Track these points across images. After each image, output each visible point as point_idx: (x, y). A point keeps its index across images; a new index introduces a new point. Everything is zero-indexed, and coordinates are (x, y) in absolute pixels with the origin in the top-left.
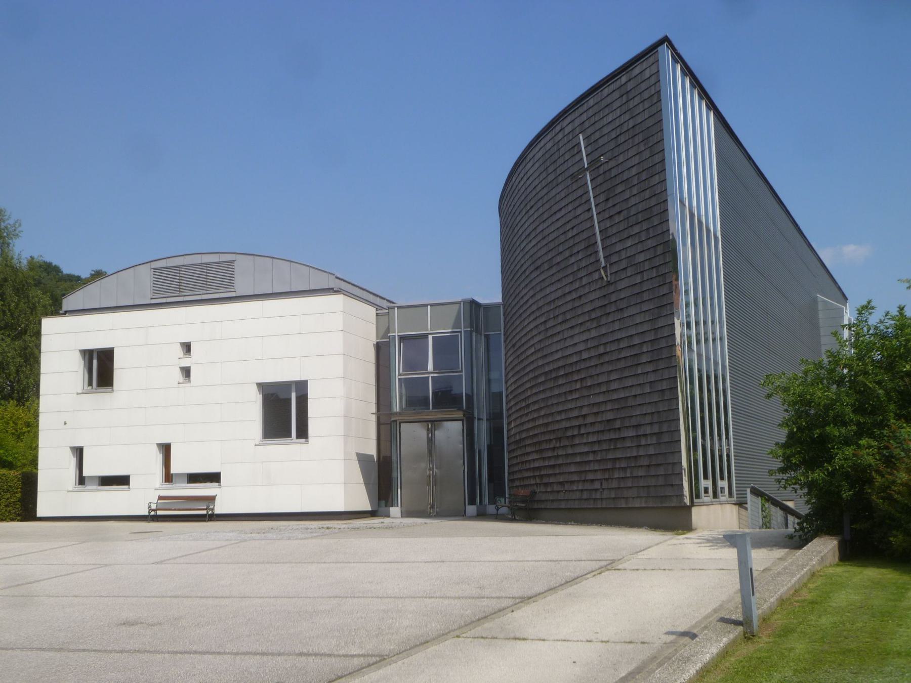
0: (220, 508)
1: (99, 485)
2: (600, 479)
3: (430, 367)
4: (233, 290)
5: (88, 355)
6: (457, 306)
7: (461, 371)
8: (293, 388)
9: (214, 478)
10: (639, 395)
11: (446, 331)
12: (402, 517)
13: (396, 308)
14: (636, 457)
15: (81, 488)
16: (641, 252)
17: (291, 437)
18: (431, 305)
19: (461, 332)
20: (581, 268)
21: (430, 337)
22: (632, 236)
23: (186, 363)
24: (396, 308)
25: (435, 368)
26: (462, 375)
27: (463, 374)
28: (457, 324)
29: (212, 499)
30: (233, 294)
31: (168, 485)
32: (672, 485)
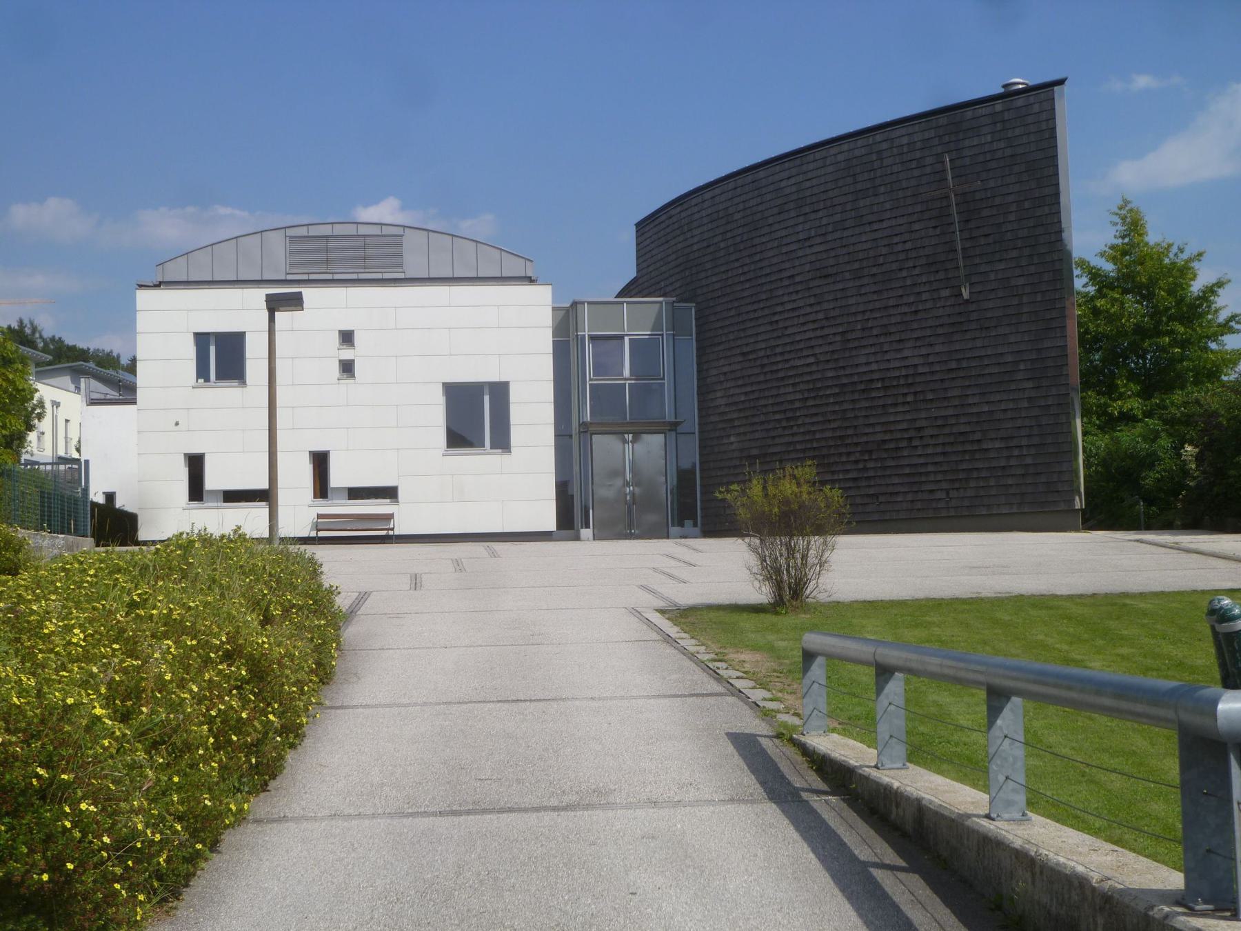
0: (402, 527)
1: (224, 502)
2: (945, 489)
3: (627, 373)
4: (401, 270)
5: (202, 340)
6: (658, 305)
7: (663, 379)
8: (486, 390)
9: (389, 493)
10: (1011, 409)
11: (644, 333)
12: (594, 539)
13: (586, 304)
14: (1004, 467)
15: (195, 504)
16: (1020, 276)
17: (484, 447)
18: (589, 303)
19: (662, 335)
20: (920, 284)
21: (626, 339)
22: (1006, 259)
23: (347, 354)
24: (586, 304)
25: (631, 375)
26: (664, 383)
27: (666, 381)
28: (657, 326)
29: (389, 517)
30: (402, 276)
31: (321, 501)
32: (1058, 492)
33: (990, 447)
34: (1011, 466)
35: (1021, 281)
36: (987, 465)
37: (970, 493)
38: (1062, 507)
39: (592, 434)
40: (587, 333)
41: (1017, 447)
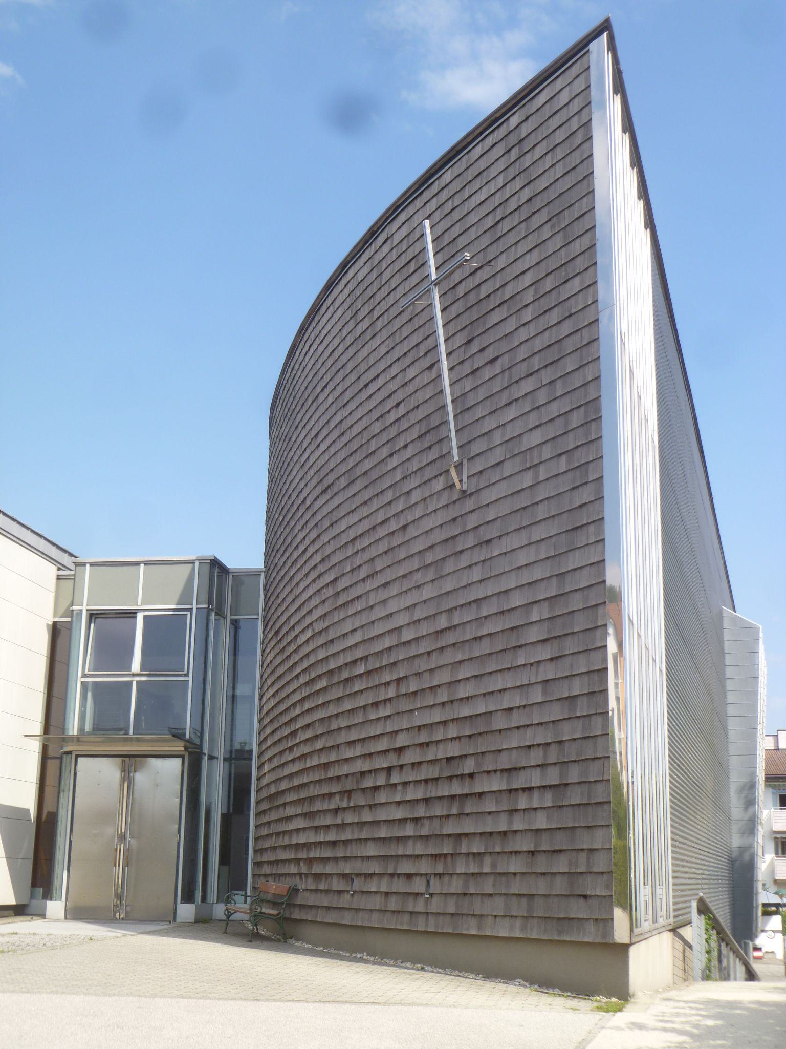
3: (136, 665)
7: (187, 675)
11: (167, 605)
13: (88, 566)
19: (191, 610)
21: (140, 616)
24: (88, 566)
25: (143, 668)
27: (190, 679)
28: (185, 596)
33: (485, 790)
34: (515, 832)
35: (536, 438)
36: (431, 851)
37: (456, 886)
38: (590, 935)
39: (77, 756)
40: (84, 608)
41: (524, 790)
